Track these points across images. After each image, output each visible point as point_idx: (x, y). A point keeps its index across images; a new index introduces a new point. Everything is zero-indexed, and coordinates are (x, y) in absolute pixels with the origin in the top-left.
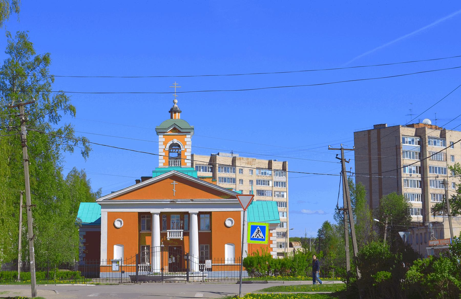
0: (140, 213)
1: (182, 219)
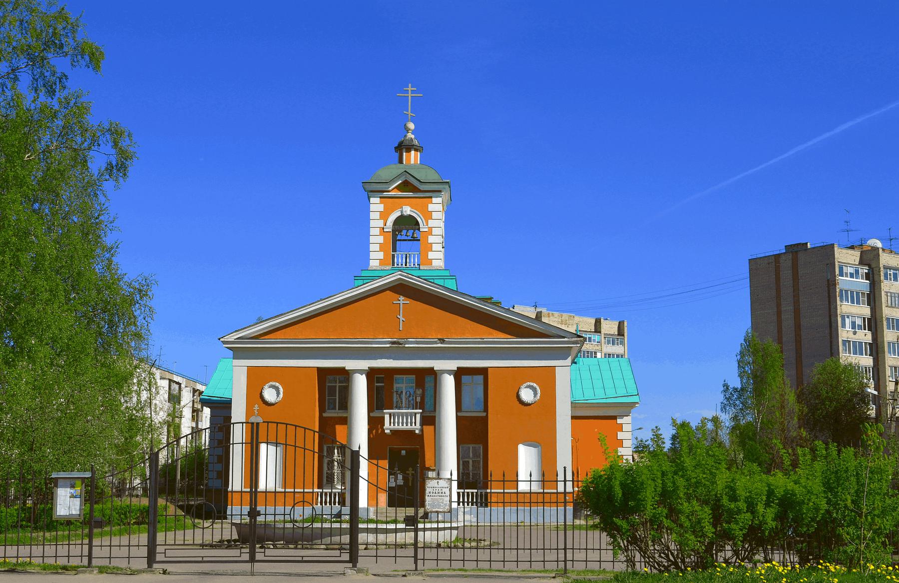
0: (320, 370)
1: (420, 384)
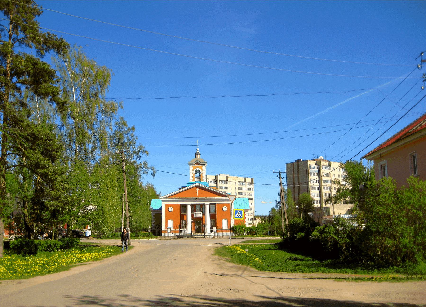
0: (181, 205)
